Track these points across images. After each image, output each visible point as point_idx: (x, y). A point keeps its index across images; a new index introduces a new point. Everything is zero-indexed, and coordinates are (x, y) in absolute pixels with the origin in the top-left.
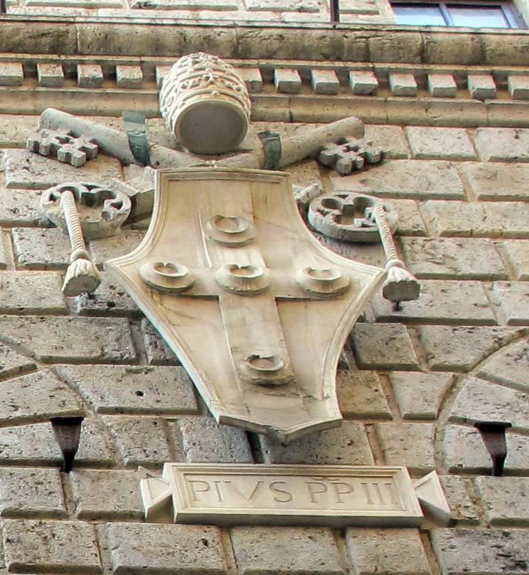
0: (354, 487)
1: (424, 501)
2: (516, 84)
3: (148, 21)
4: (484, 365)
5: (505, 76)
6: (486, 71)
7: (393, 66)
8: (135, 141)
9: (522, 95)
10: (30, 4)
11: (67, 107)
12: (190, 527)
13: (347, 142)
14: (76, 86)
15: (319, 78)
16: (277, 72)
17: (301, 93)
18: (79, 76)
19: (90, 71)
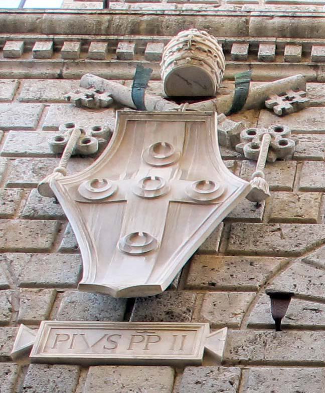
0: (162, 337)
1: (207, 349)
2: (316, 51)
3: (76, 12)
4: (59, 243)
5: (310, 46)
6: (78, 39)
7: (149, 37)
8: (136, 99)
9: (318, 60)
10: (268, 3)
11: (98, 73)
12: (38, 366)
13: (286, 95)
14: (256, 60)
15: (289, 51)
16: (261, 47)
17: (277, 62)
18: (259, 54)
19: (266, 50)
